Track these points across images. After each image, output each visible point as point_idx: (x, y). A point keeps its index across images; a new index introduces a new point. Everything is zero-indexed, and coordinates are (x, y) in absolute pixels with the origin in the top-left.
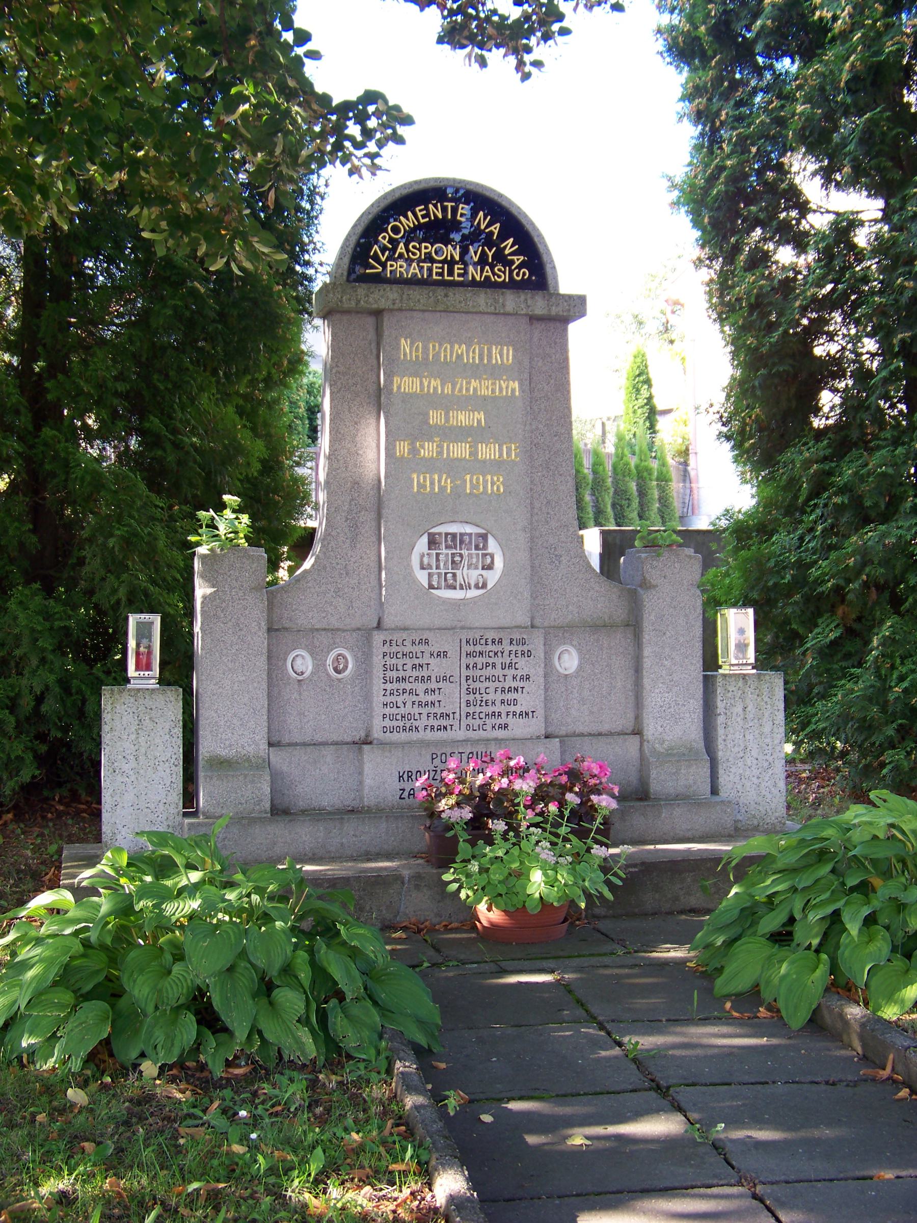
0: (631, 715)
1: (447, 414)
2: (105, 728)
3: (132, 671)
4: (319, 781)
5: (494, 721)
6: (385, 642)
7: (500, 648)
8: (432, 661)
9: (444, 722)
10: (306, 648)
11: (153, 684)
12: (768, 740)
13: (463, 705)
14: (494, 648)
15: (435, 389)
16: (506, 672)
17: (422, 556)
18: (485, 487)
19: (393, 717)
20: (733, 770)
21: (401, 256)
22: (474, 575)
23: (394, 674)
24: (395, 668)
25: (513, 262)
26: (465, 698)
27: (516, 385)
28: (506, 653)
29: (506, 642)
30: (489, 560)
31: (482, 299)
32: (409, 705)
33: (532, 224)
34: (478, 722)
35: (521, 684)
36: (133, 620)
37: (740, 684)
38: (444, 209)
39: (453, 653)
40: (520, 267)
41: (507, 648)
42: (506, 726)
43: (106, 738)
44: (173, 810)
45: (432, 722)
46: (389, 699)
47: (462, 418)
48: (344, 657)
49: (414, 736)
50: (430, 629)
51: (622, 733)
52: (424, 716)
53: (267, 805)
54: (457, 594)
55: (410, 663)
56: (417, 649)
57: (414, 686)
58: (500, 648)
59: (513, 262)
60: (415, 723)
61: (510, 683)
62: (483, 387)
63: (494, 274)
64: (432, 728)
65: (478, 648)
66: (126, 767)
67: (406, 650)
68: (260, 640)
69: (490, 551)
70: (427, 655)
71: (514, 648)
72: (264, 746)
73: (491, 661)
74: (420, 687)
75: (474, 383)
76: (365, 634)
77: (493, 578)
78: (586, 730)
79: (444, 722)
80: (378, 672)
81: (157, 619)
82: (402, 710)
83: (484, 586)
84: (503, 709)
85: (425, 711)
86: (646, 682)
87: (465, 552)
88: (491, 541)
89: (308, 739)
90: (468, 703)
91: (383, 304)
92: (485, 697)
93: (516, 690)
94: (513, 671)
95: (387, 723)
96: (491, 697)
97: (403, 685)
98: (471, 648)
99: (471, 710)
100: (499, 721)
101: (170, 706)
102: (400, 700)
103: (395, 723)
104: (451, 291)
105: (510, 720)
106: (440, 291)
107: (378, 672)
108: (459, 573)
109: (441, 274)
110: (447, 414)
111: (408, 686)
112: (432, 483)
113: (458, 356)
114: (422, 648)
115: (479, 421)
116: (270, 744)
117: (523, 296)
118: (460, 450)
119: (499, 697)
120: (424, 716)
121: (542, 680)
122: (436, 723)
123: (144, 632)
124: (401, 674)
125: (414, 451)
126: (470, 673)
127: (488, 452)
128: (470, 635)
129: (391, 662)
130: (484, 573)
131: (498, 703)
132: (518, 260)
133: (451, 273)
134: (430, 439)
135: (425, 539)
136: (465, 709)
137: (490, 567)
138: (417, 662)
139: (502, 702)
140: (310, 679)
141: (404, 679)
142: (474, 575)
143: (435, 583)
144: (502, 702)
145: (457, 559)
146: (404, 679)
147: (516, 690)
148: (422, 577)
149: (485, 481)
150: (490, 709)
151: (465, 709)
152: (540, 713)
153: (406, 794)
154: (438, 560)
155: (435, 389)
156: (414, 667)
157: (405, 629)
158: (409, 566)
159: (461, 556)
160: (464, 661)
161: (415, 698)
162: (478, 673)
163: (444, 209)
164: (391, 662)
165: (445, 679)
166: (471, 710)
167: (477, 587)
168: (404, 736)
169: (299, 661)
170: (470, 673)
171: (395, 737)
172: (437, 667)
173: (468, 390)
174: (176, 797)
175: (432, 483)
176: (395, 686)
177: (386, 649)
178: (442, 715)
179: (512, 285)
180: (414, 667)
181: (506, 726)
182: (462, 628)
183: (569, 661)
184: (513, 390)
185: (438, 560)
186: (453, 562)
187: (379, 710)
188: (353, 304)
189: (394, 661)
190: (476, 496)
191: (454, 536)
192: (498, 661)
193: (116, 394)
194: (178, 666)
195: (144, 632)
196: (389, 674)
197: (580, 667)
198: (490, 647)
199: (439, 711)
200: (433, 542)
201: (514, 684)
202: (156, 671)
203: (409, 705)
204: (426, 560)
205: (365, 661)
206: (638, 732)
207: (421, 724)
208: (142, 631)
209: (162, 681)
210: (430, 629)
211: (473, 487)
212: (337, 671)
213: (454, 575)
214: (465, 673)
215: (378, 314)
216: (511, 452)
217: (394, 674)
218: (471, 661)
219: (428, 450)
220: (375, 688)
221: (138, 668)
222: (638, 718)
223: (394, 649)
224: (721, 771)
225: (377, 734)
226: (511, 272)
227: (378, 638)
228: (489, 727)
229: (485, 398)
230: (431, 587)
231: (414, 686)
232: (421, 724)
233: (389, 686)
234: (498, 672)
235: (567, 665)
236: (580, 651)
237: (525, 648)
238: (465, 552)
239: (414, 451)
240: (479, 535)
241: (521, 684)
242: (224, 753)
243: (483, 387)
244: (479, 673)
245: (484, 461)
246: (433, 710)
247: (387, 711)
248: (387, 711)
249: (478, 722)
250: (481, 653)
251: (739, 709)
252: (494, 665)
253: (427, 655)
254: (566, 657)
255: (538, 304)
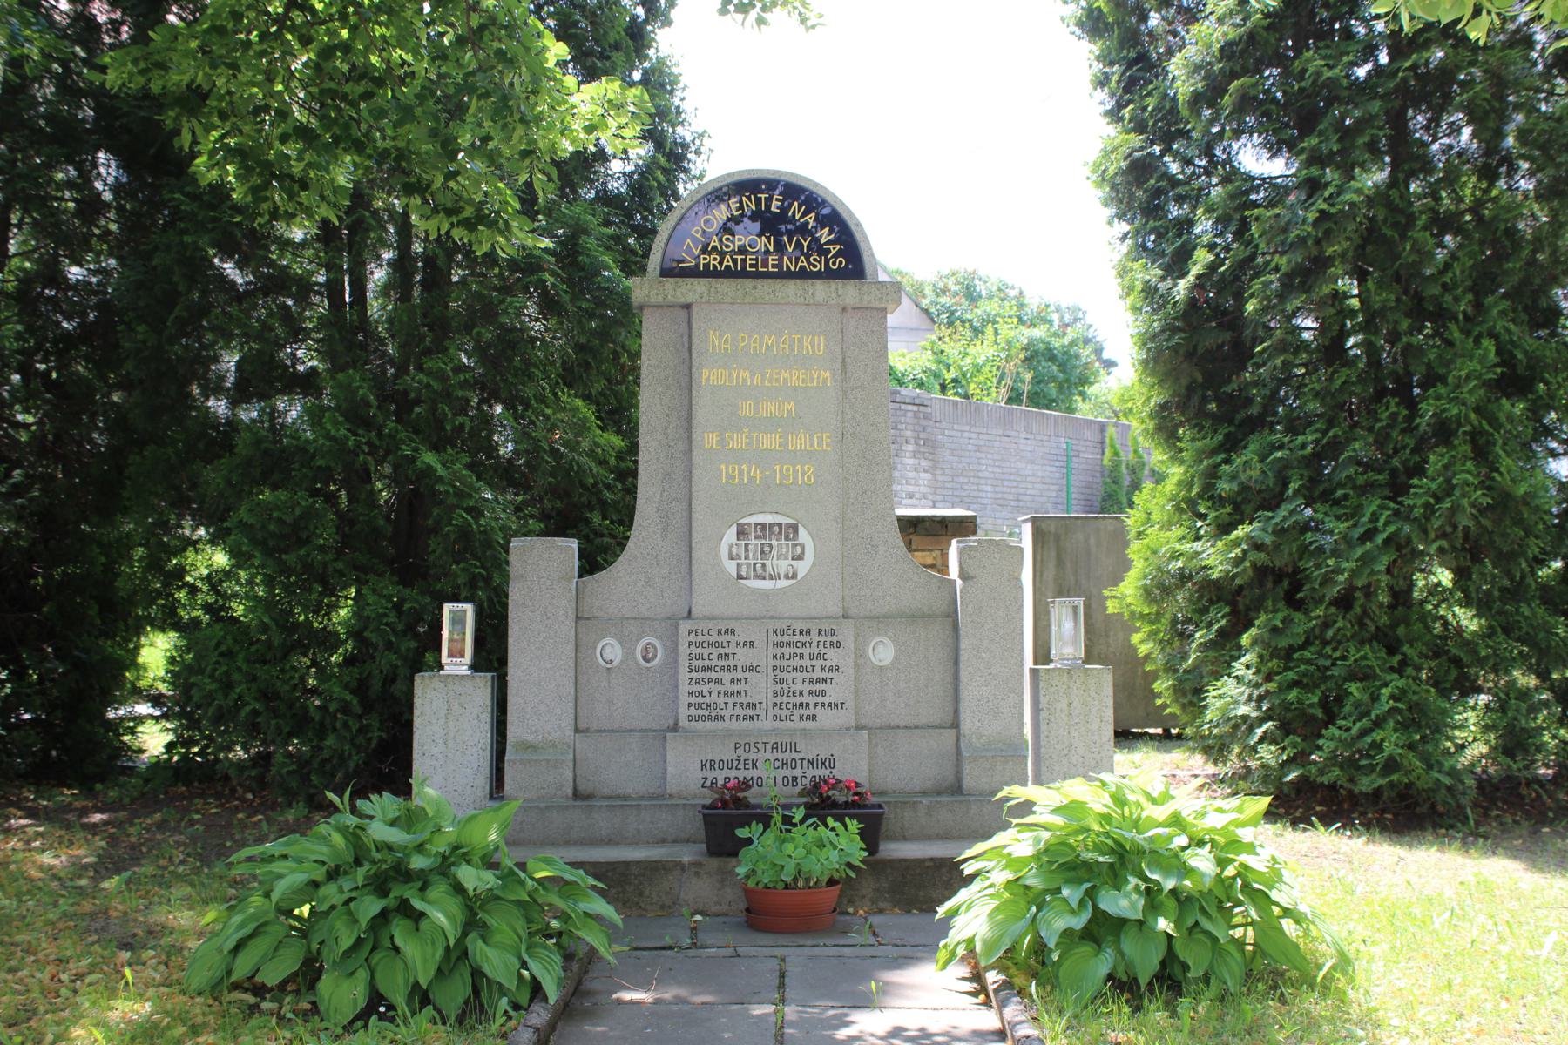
0: (950, 709)
1: (756, 404)
2: (416, 712)
3: (445, 659)
4: (621, 770)
5: (801, 711)
6: (690, 632)
7: (808, 638)
8: (739, 651)
9: (750, 712)
10: (615, 636)
11: (464, 670)
12: (1095, 738)
13: (770, 695)
14: (802, 638)
15: (745, 380)
16: (814, 662)
17: (731, 546)
18: (795, 478)
19: (698, 706)
20: (1057, 768)
21: (714, 248)
22: (783, 566)
23: (700, 663)
24: (700, 657)
25: (829, 251)
26: (772, 688)
27: (828, 374)
28: (814, 644)
29: (814, 632)
30: (799, 550)
31: (792, 288)
32: (715, 694)
33: (850, 211)
34: (785, 712)
35: (830, 675)
36: (447, 607)
37: (1065, 678)
38: (758, 201)
39: (760, 643)
40: (836, 256)
41: (816, 638)
42: (814, 717)
43: (417, 722)
44: (480, 793)
45: (738, 711)
46: (694, 688)
47: (770, 409)
48: (654, 646)
49: (720, 725)
50: (737, 619)
51: (940, 727)
52: (730, 706)
53: (570, 791)
54: (767, 584)
55: (715, 652)
56: (721, 638)
57: (720, 675)
58: (808, 638)
59: (829, 251)
60: (721, 713)
61: (818, 674)
62: (796, 377)
63: (809, 263)
64: (738, 717)
65: (786, 638)
66: (435, 751)
67: (712, 639)
68: (567, 628)
69: (800, 540)
70: (733, 644)
71: (822, 638)
72: (569, 732)
73: (798, 651)
74: (727, 677)
75: (785, 374)
76: (672, 622)
77: (802, 568)
78: (903, 723)
79: (750, 712)
80: (684, 661)
81: (469, 608)
82: (708, 699)
83: (794, 576)
84: (812, 700)
85: (730, 700)
86: (963, 675)
87: (775, 543)
88: (801, 530)
89: (616, 726)
90: (775, 693)
91: (689, 299)
92: (793, 687)
93: (825, 680)
94: (821, 662)
95: (692, 711)
96: (798, 687)
97: (708, 675)
98: (778, 639)
99: (778, 700)
100: (806, 712)
101: (481, 689)
102: (705, 688)
103: (700, 712)
104: (760, 282)
105: (819, 711)
106: (748, 283)
107: (684, 661)
108: (768, 563)
109: (755, 266)
110: (756, 404)
111: (714, 676)
112: (741, 474)
113: (768, 348)
114: (728, 637)
115: (789, 412)
116: (577, 730)
117: (835, 284)
118: (770, 441)
119: (807, 687)
120: (730, 706)
121: (852, 671)
122: (742, 713)
123: (458, 620)
124: (707, 663)
125: (723, 442)
126: (777, 663)
127: (798, 442)
128: (779, 625)
129: (696, 651)
130: (794, 563)
131: (806, 693)
132: (834, 249)
133: (765, 264)
134: (740, 430)
135: (734, 529)
136: (772, 699)
137: (800, 558)
138: (722, 651)
139: (811, 693)
140: (618, 667)
141: (709, 668)
142: (783, 566)
143: (744, 574)
144: (811, 693)
145: (767, 549)
146: (709, 668)
147: (825, 680)
148: (731, 567)
149: (795, 471)
150: (798, 700)
151: (772, 699)
152: (850, 704)
153: (708, 783)
154: (747, 550)
155: (745, 380)
156: (720, 656)
157: (713, 618)
158: (717, 555)
159: (771, 546)
160: (771, 651)
161: (720, 687)
162: (785, 663)
163: (758, 201)
164: (696, 651)
165: (751, 669)
166: (778, 700)
167: (787, 577)
168: (709, 725)
169: (608, 650)
170: (777, 663)
171: (700, 725)
172: (743, 657)
173: (778, 380)
174: (482, 782)
175: (741, 474)
176: (701, 675)
177: (692, 638)
178: (748, 705)
179: (828, 275)
180: (720, 656)
181: (814, 717)
182: (772, 618)
183: (883, 652)
184: (825, 380)
185: (747, 550)
186: (762, 552)
187: (684, 699)
188: (660, 299)
189: (700, 650)
190: (786, 486)
191: (763, 526)
192: (806, 651)
193: (1330, 379)
194: (491, 653)
195: (458, 620)
196: (695, 663)
197: (896, 659)
198: (798, 638)
199: (827, 700)
200: (741, 533)
201: (823, 675)
202: (468, 658)
203: (715, 694)
204: (734, 550)
205: (673, 650)
206: (955, 725)
207: (727, 713)
208: (458, 621)
209: (475, 667)
210: (737, 619)
211: (783, 477)
212: (645, 658)
213: (764, 565)
214: (772, 663)
215: (687, 307)
216: (824, 442)
217: (700, 663)
218: (778, 651)
219: (737, 441)
220: (681, 677)
221: (450, 655)
222: (956, 712)
223: (700, 638)
224: (1044, 769)
225: (683, 722)
226: (827, 261)
227: (684, 626)
228: (796, 718)
229: (795, 389)
230: (740, 577)
231: (720, 675)
232: (727, 713)
233: (694, 675)
234: (806, 662)
235: (881, 656)
236: (895, 642)
237: (834, 639)
238: (775, 543)
239: (723, 442)
240: (790, 525)
241: (830, 675)
242: (530, 738)
243: (796, 377)
244: (786, 663)
245: (795, 452)
246: (739, 700)
247: (693, 700)
248: (693, 700)
249: (785, 712)
250: (788, 643)
251: (1064, 705)
252: (802, 656)
253: (733, 644)
254: (880, 648)
255: (849, 291)
